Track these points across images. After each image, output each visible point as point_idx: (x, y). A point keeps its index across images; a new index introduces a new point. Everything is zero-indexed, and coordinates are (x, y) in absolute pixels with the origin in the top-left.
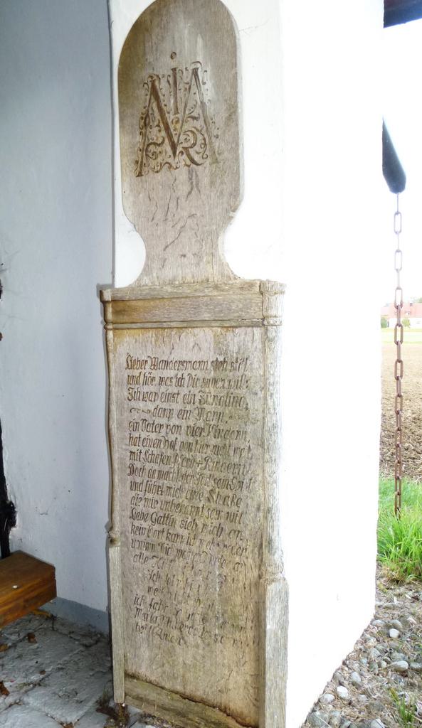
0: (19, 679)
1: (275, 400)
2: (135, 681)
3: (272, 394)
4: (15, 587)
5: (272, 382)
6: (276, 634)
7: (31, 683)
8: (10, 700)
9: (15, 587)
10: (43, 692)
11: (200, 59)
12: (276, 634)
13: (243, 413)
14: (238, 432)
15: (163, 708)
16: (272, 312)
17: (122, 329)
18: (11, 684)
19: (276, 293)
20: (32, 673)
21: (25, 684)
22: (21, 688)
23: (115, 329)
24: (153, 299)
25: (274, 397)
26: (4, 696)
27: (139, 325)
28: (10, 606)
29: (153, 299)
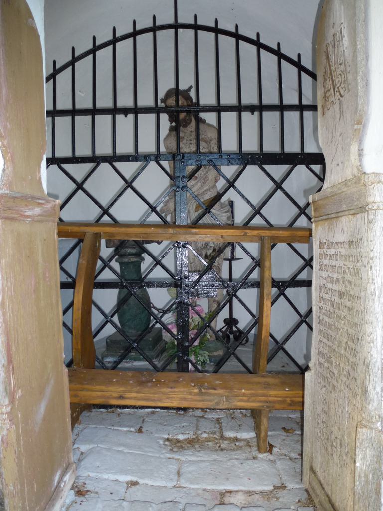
0: (284, 450)
1: (374, 272)
2: (313, 475)
3: (371, 267)
4: (287, 389)
5: (371, 257)
6: (366, 476)
7: (289, 456)
8: (271, 457)
9: (287, 389)
10: (289, 463)
11: (342, 21)
12: (366, 476)
13: (359, 282)
14: (357, 297)
15: (320, 503)
16: (370, 199)
17: (332, 218)
18: (279, 450)
19: (372, 183)
20: (294, 452)
21: (285, 455)
22: (282, 455)
23: (315, 221)
24: (333, 196)
25: (373, 269)
26: (269, 453)
27: (324, 217)
28: (279, 399)
29: (333, 196)
